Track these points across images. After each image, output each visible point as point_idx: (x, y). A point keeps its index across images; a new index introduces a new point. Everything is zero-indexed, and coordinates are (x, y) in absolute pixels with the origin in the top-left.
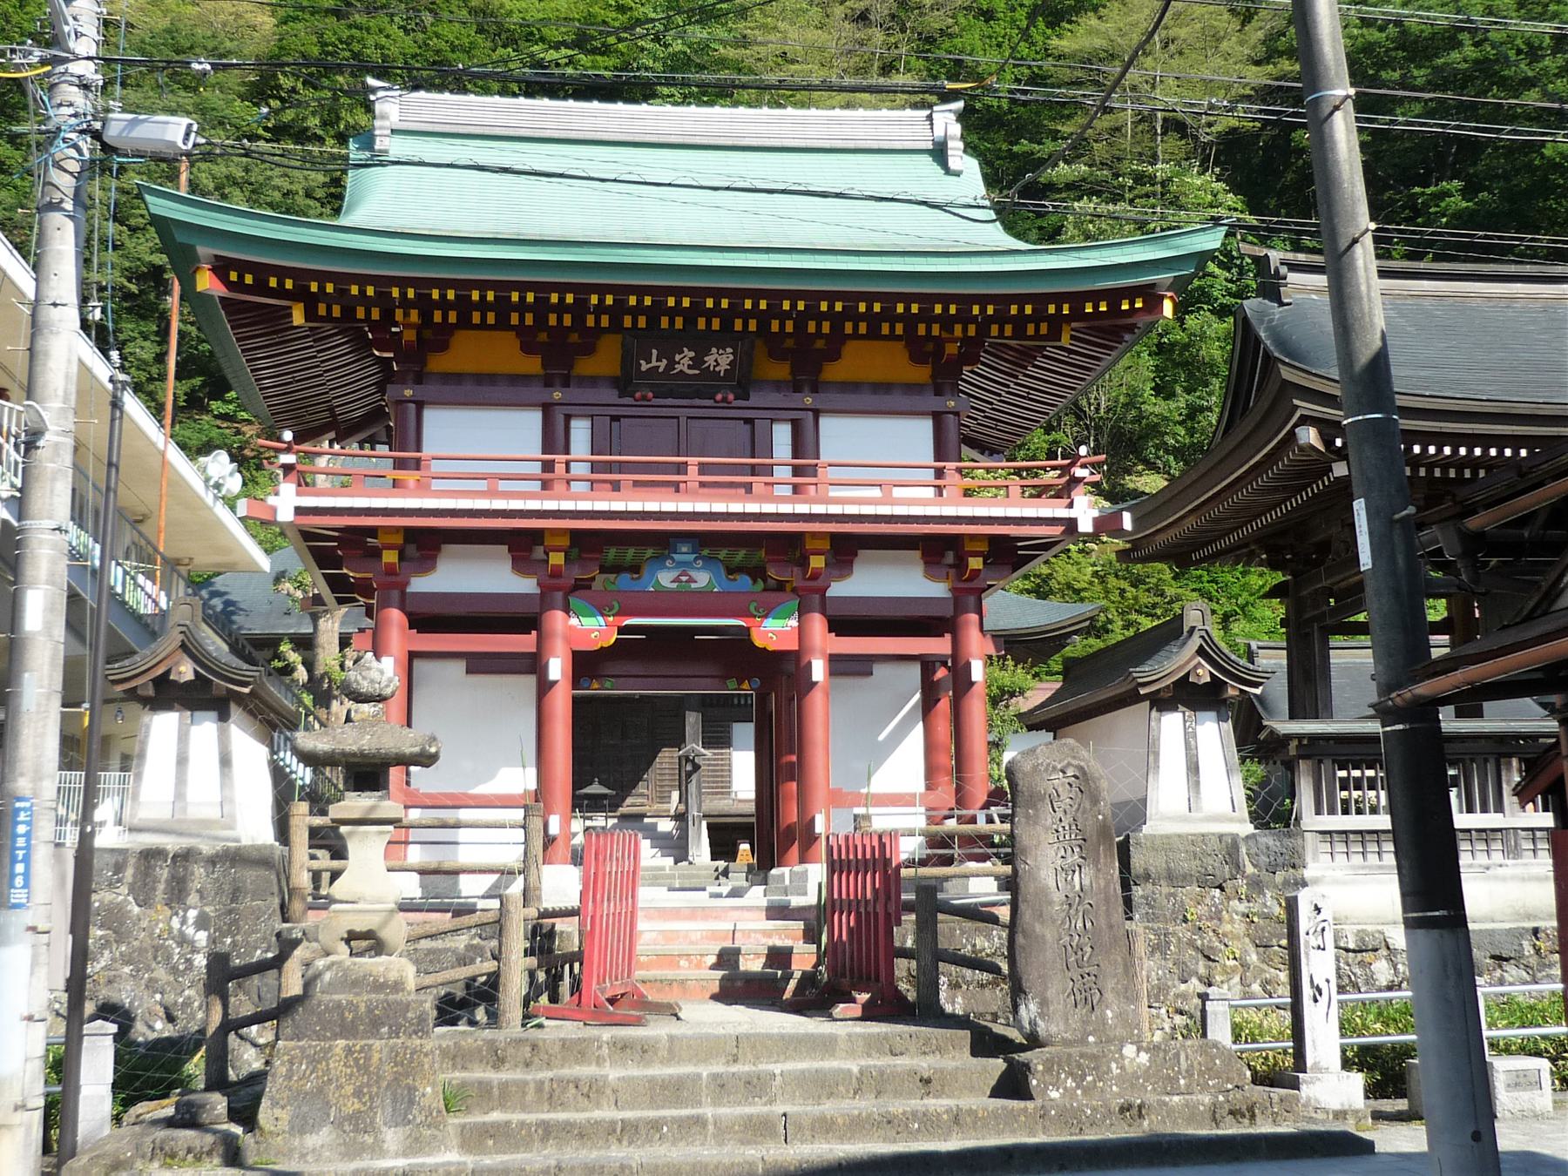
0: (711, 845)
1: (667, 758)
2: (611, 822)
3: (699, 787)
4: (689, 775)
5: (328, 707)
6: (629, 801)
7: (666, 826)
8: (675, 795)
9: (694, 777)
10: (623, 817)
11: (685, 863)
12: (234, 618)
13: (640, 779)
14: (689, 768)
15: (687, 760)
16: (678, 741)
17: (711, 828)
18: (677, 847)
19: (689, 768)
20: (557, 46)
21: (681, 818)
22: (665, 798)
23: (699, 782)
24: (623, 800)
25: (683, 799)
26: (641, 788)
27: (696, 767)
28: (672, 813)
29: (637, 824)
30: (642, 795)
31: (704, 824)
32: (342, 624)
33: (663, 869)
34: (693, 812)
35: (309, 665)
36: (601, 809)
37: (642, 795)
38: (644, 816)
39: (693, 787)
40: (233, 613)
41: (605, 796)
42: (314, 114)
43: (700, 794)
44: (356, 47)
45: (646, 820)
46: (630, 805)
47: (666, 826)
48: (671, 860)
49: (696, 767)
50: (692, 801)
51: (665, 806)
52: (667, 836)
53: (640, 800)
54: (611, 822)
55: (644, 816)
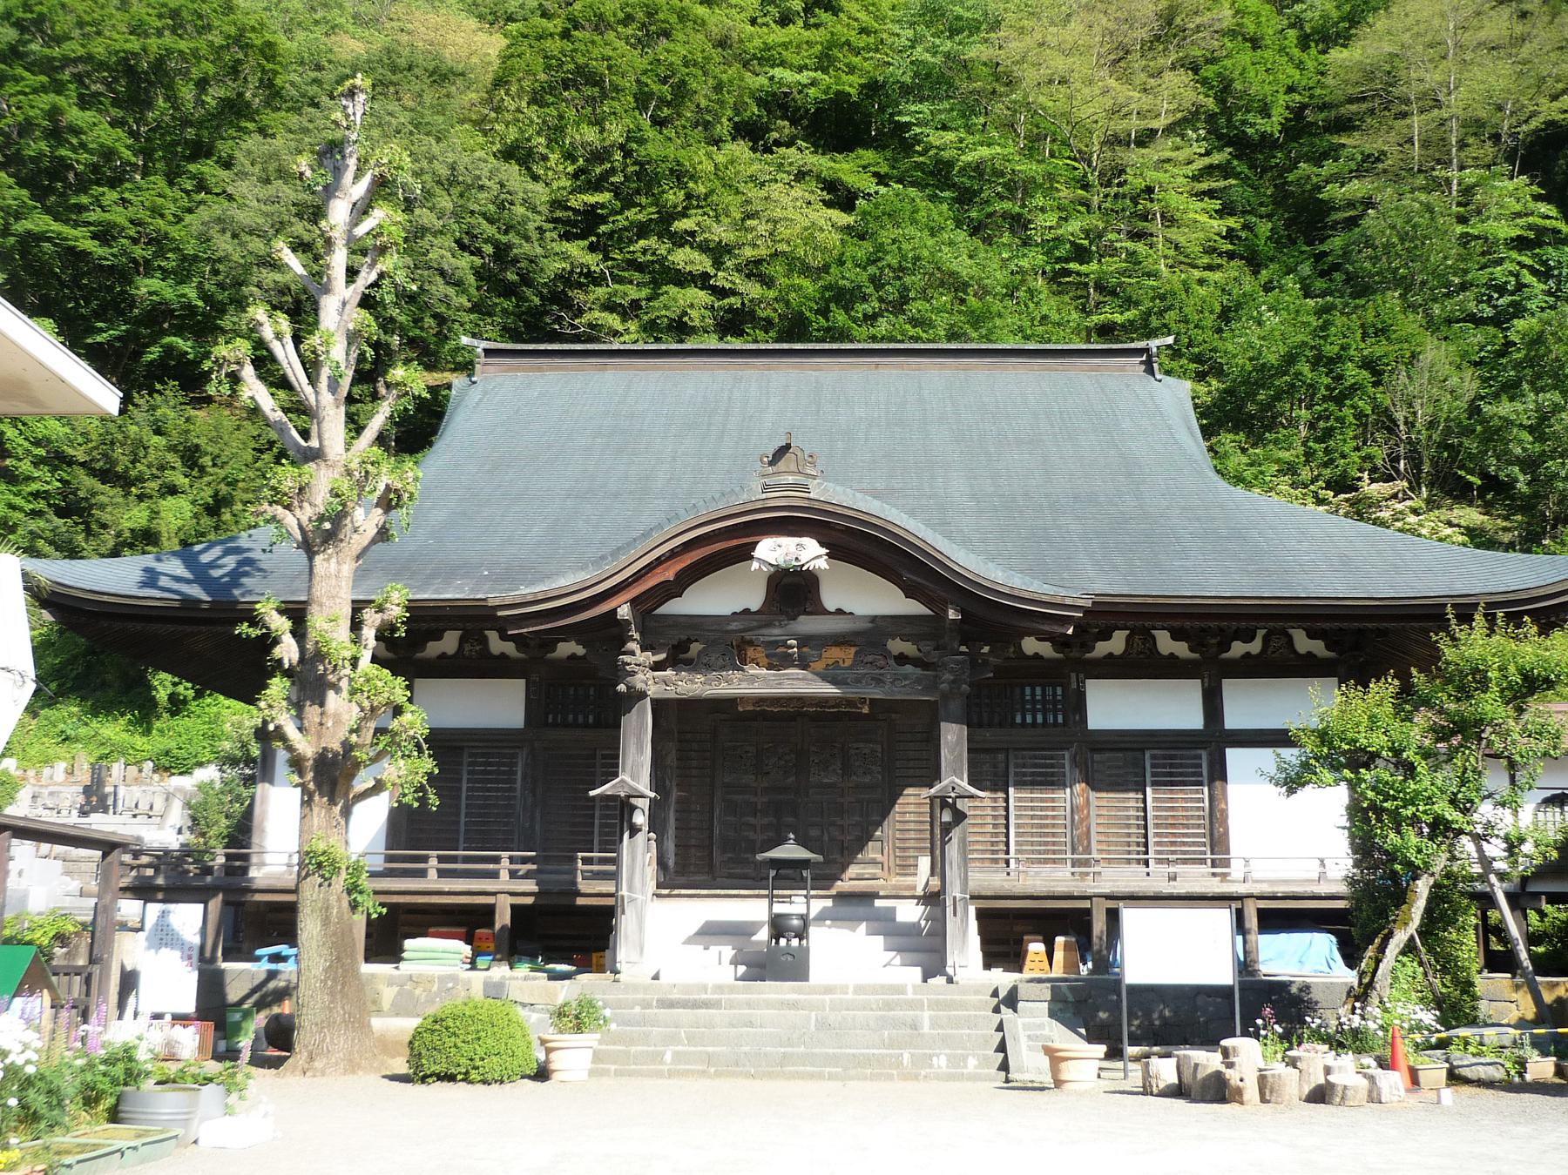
0: (981, 933)
1: (912, 803)
2: (817, 906)
3: (964, 852)
4: (947, 829)
5: (322, 705)
6: (853, 870)
7: (910, 912)
8: (924, 863)
9: (956, 834)
10: (842, 897)
11: (940, 980)
12: (244, 580)
13: (870, 838)
14: (947, 817)
15: (944, 804)
16: (931, 775)
17: (982, 915)
18: (926, 949)
19: (947, 817)
20: (800, 69)
21: (933, 899)
22: (908, 868)
23: (963, 841)
24: (844, 868)
25: (938, 868)
26: (872, 851)
27: (959, 817)
28: (919, 892)
29: (861, 910)
30: (874, 862)
31: (972, 910)
32: (359, 576)
33: (900, 989)
34: (954, 891)
35: (299, 633)
36: (799, 883)
37: (874, 862)
38: (874, 896)
39: (953, 851)
40: (246, 574)
41: (805, 863)
42: (539, 134)
43: (965, 862)
44: (581, 60)
45: (878, 903)
46: (853, 878)
47: (910, 912)
48: (917, 972)
49: (959, 817)
50: (953, 874)
51: (909, 880)
52: (911, 930)
53: (869, 870)
54: (817, 906)
55: (874, 896)
